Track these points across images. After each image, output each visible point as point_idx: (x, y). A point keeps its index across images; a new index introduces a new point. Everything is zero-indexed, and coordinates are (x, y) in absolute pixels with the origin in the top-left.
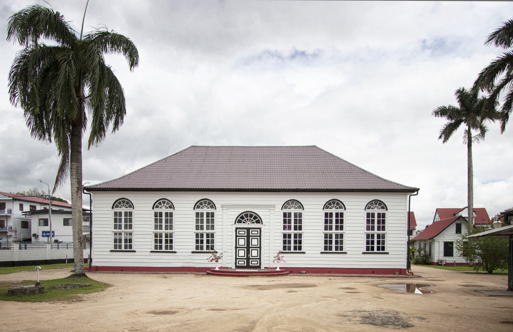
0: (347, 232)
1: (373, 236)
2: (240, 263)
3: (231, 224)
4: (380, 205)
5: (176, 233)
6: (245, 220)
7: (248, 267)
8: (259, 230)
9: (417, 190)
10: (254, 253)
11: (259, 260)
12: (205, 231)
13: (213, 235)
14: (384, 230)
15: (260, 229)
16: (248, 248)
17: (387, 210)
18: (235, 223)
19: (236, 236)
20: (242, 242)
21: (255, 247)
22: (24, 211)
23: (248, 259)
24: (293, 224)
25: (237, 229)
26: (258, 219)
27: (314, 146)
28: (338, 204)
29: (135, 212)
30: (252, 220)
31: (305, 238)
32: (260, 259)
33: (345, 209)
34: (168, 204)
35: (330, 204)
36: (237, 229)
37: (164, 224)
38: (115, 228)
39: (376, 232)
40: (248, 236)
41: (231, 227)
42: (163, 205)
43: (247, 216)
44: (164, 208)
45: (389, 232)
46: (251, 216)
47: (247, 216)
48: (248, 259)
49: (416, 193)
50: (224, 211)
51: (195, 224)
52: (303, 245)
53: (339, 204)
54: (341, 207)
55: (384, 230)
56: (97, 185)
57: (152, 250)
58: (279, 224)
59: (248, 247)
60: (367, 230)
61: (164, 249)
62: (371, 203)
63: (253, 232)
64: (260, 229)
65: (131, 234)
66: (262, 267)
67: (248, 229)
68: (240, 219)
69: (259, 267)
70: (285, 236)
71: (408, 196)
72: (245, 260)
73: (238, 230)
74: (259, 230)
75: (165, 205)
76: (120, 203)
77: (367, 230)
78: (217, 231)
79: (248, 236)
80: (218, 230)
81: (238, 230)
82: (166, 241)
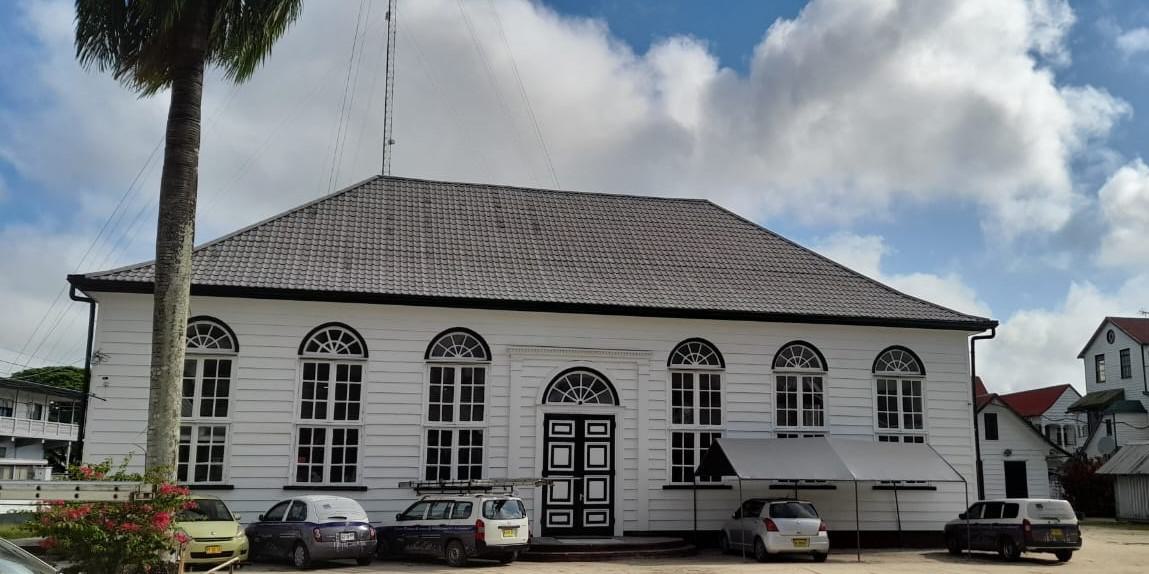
0: (931, 433)
1: (447, 435)
2: (555, 519)
3: (530, 402)
4: (705, 352)
5: (369, 430)
6: (571, 393)
7: (578, 530)
8: (608, 422)
9: (993, 325)
10: (596, 490)
11: (608, 511)
12: (457, 424)
13: (478, 437)
14: (224, 414)
15: (612, 418)
16: (579, 471)
17: (923, 372)
18: (544, 402)
19: (547, 439)
20: (562, 456)
21: (597, 473)
22: (304, 356)
23: (578, 507)
24: (331, 402)
25: (548, 417)
26: (603, 389)
27: (705, 201)
28: (807, 355)
29: (927, 387)
30: (590, 394)
31: (236, 439)
32: (611, 506)
33: (826, 368)
34: (347, 339)
35: (685, 351)
36: (548, 417)
37: (457, 403)
38: (677, 419)
39: (330, 423)
40: (580, 440)
41: (530, 412)
42: (330, 342)
43: (575, 381)
44: (333, 353)
45: (833, 431)
46: (587, 381)
47: (575, 381)
48: (578, 507)
49: (989, 332)
50: (516, 366)
51: (426, 403)
52: (360, 464)
53: (813, 356)
54: (814, 364)
55: (224, 414)
56: (117, 273)
57: (290, 484)
58: (661, 406)
59: (579, 471)
60: (881, 426)
61: (327, 481)
62: (785, 351)
63: (593, 429)
64: (612, 418)
65: (220, 431)
66: (618, 530)
67: (580, 419)
68: (558, 388)
69: (608, 532)
70: (305, 434)
71: (970, 338)
72: (571, 512)
73: (551, 422)
74: (608, 422)
75: (339, 342)
76: (447, 343)
77: (881, 426)
78: (491, 425)
79: (580, 440)
80: (494, 421)
81: (551, 422)
82: (337, 455)
